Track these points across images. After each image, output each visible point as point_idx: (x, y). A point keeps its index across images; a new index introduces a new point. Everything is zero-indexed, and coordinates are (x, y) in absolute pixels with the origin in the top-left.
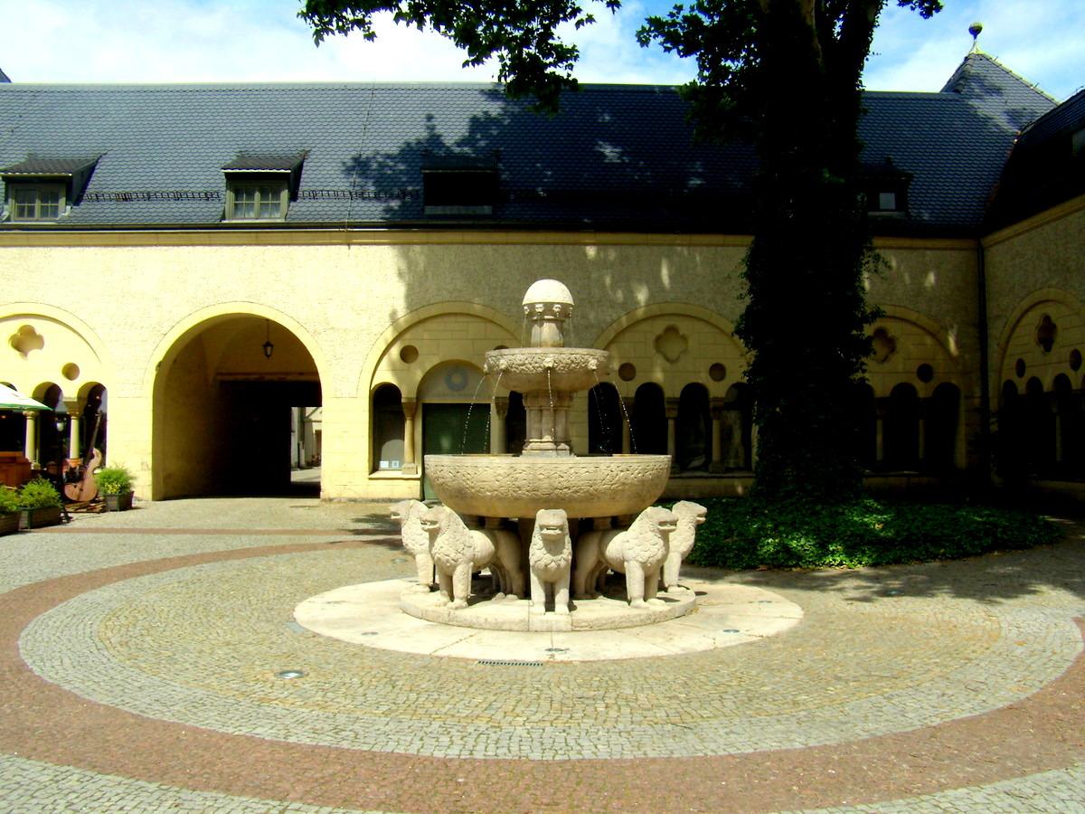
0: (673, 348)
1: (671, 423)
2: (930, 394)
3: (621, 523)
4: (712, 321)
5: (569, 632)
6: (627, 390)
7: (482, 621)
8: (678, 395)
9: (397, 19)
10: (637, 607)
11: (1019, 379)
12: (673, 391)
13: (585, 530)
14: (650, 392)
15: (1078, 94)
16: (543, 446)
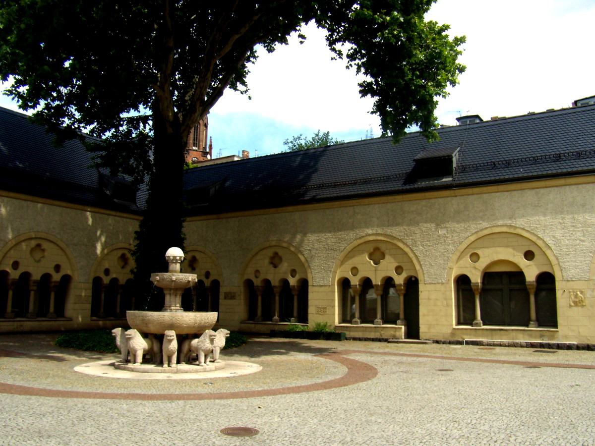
0: (38, 255)
1: (32, 293)
2: (17, 277)
3: (197, 336)
4: (58, 243)
5: (213, 371)
6: (106, 280)
7: (191, 369)
8: (39, 278)
9: (330, 49)
10: (202, 366)
11: (14, 271)
12: (36, 276)
13: (183, 339)
14: (26, 276)
15: (361, 141)
16: (177, 308)
